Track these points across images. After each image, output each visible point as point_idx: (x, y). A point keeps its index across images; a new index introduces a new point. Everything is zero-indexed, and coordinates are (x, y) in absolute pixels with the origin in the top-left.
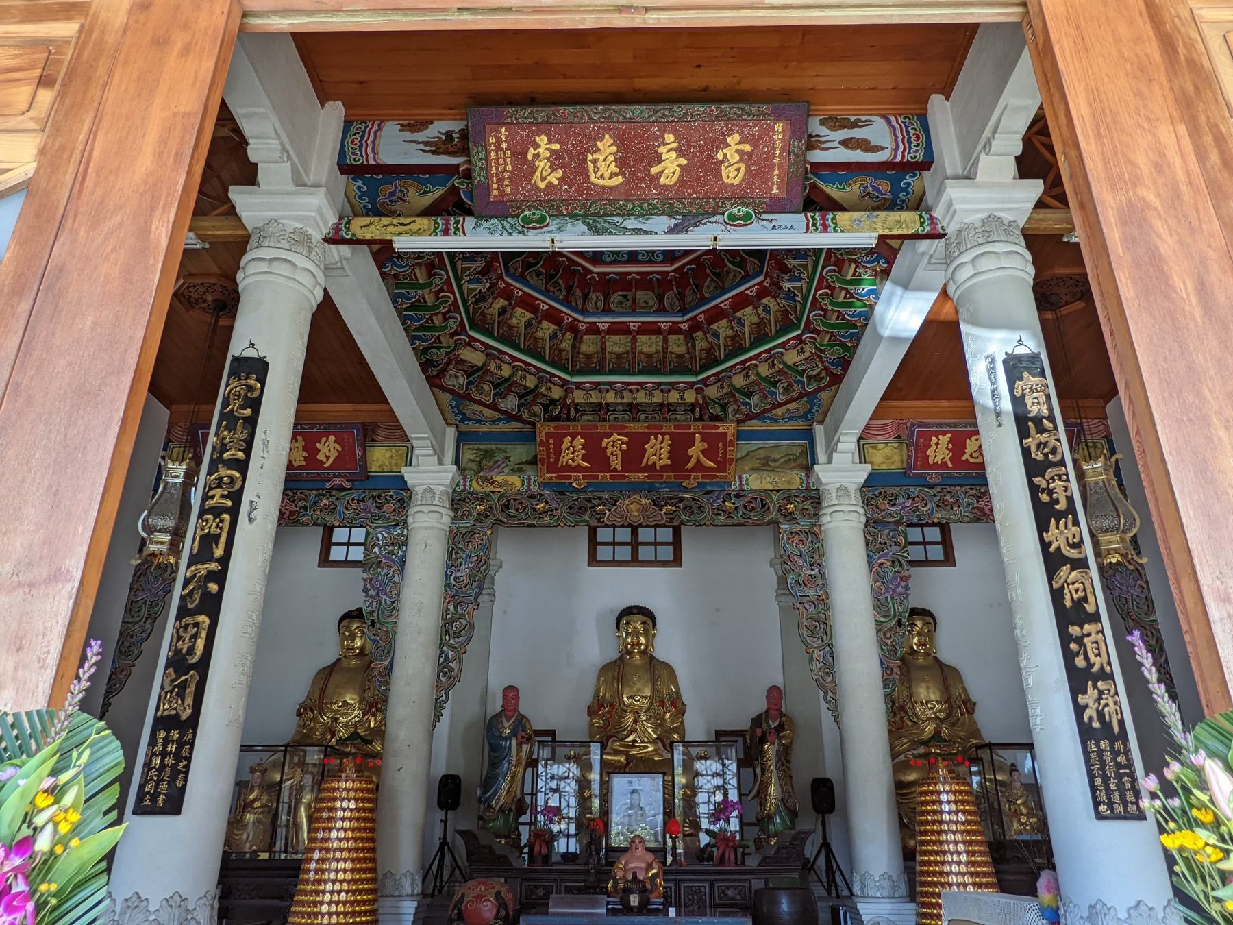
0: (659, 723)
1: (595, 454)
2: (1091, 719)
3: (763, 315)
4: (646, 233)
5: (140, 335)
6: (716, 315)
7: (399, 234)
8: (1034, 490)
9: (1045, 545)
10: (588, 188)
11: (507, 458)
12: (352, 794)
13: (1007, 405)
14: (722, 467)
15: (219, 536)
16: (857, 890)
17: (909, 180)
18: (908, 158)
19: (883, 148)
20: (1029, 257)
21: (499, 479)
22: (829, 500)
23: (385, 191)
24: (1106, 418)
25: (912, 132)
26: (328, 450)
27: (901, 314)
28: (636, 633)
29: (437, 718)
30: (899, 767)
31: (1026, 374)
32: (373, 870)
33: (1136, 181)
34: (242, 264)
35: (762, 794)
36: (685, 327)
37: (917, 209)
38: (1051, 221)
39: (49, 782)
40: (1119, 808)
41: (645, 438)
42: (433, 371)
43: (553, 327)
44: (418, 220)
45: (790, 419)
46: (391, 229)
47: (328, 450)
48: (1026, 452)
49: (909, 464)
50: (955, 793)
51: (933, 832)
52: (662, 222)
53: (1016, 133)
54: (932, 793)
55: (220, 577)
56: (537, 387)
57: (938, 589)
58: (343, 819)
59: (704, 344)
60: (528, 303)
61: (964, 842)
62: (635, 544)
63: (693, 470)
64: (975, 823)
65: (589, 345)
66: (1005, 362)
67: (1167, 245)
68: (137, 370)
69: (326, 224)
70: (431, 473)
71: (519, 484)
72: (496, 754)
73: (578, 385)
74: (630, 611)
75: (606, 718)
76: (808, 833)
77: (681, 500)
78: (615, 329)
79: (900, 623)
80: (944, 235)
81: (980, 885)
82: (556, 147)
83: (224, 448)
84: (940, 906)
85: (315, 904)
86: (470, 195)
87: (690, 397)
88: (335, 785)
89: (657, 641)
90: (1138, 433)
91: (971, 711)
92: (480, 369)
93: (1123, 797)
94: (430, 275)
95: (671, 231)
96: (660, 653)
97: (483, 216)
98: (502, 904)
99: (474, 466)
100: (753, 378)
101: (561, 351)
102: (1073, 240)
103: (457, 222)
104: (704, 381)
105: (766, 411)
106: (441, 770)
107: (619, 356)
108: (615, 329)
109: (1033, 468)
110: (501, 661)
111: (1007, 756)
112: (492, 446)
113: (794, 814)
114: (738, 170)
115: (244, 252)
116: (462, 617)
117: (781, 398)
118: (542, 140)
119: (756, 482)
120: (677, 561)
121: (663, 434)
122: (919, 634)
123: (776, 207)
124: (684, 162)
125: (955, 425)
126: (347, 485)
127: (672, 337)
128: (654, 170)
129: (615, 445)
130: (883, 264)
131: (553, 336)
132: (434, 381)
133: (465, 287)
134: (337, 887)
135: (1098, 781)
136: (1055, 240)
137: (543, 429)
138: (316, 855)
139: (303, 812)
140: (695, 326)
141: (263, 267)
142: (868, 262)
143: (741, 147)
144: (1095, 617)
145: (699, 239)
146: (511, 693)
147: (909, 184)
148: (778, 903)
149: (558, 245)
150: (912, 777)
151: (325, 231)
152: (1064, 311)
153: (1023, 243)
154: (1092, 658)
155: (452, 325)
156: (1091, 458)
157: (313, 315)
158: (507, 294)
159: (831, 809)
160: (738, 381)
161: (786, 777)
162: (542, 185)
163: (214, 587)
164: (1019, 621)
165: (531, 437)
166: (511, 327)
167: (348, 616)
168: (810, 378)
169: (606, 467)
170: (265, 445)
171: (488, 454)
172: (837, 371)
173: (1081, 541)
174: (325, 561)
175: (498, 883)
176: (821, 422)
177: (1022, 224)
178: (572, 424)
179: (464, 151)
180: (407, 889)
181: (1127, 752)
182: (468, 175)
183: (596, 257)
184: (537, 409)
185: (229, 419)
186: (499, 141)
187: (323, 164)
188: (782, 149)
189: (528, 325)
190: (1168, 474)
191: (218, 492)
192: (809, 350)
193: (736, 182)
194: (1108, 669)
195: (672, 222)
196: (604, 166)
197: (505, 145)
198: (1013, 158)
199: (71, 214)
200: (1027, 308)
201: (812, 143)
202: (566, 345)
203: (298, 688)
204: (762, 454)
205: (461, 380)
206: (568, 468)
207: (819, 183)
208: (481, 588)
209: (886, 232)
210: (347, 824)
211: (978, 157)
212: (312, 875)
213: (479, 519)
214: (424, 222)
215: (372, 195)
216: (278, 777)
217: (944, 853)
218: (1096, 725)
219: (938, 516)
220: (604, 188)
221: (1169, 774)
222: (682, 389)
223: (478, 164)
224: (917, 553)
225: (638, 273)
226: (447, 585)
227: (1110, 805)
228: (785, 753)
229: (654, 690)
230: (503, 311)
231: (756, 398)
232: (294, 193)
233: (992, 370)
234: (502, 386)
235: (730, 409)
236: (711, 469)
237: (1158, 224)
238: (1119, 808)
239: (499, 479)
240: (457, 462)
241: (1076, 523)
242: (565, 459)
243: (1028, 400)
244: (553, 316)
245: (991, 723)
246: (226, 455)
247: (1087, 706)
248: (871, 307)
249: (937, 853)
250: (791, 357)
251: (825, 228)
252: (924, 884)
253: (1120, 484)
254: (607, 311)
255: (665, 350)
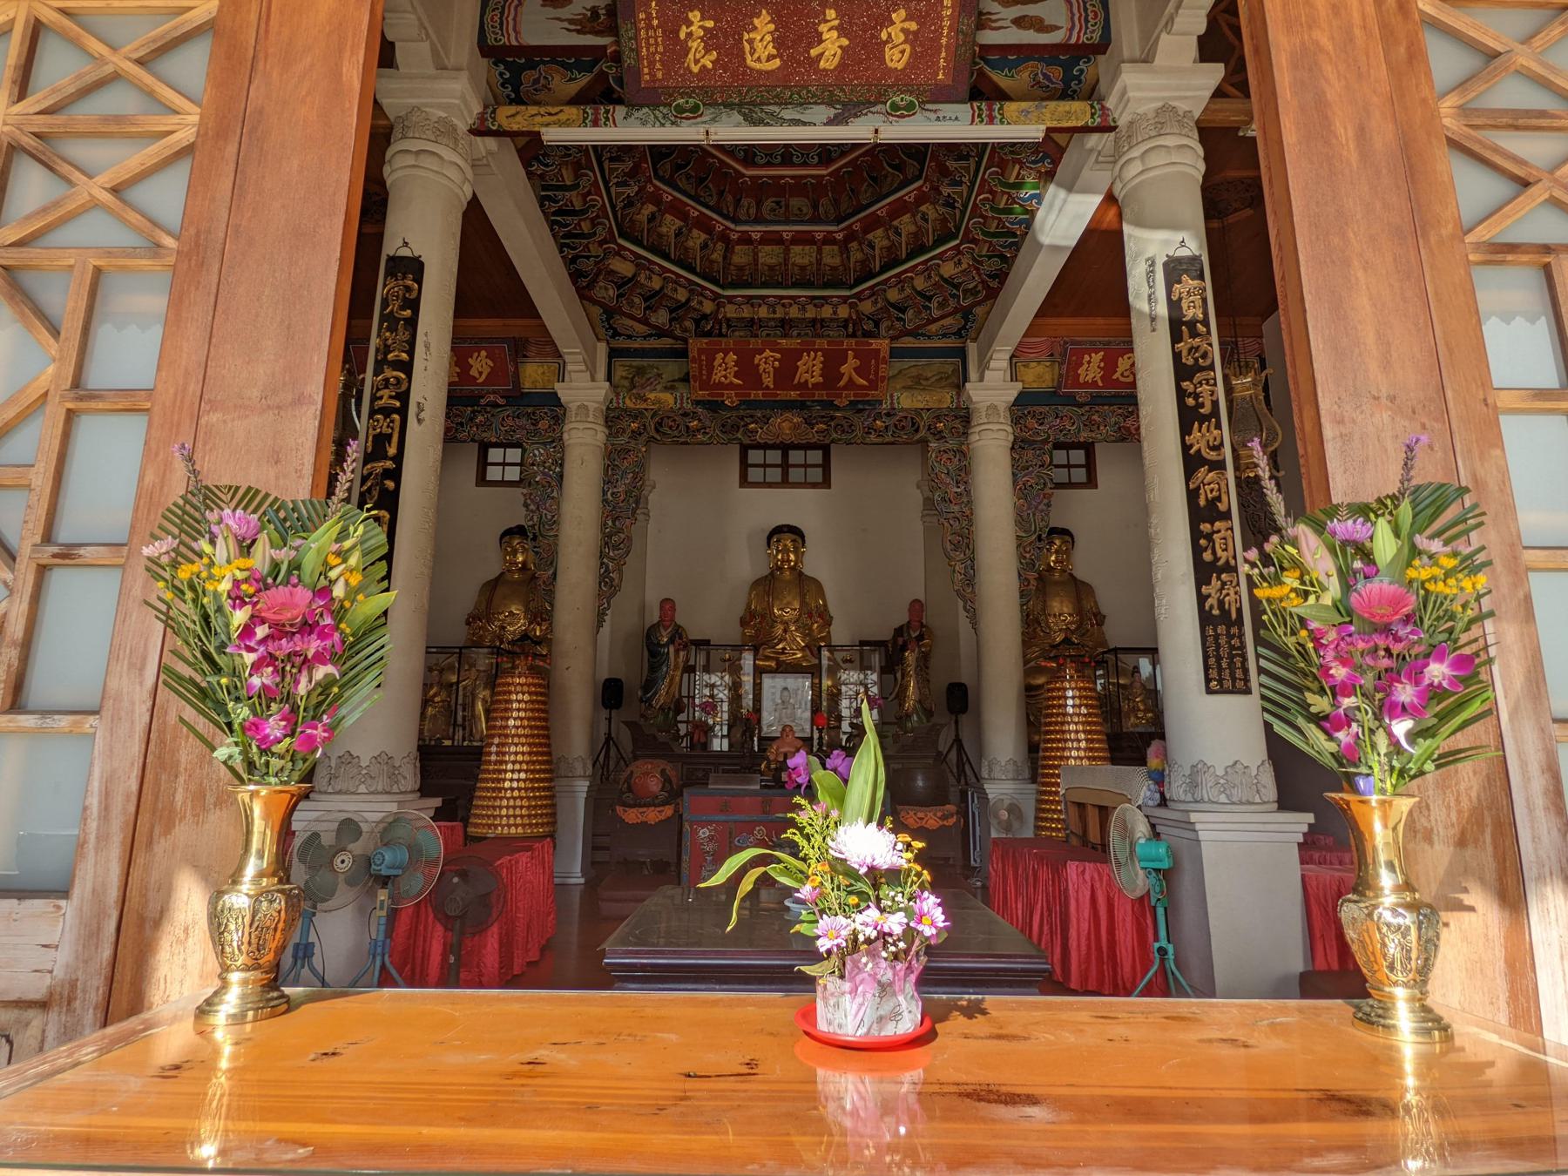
0: (806, 632)
1: (747, 370)
2: (1211, 607)
3: (921, 222)
4: (805, 124)
5: (346, 178)
6: (872, 223)
7: (547, 125)
8: (1181, 394)
9: (1186, 448)
10: (744, 73)
11: (659, 375)
12: (525, 689)
13: (1162, 310)
14: (873, 385)
15: (390, 436)
16: (985, 774)
17: (1082, 66)
18: (1083, 39)
19: (1058, 28)
20: (1201, 151)
21: (652, 396)
22: (979, 418)
23: (528, 77)
24: (1261, 337)
25: (1090, 8)
26: (480, 365)
27: (1062, 218)
28: (786, 551)
29: (600, 623)
30: (1030, 670)
31: (1185, 277)
32: (549, 754)
33: (1312, 23)
34: (388, 157)
35: (901, 696)
36: (840, 236)
37: (1089, 98)
38: (1229, 112)
39: (336, 547)
40: (1228, 684)
41: (798, 355)
42: (583, 282)
43: (704, 236)
44: (566, 108)
45: (944, 335)
46: (538, 119)
47: (480, 365)
48: (1177, 356)
49: (1060, 383)
50: (1079, 689)
51: (1056, 723)
52: (822, 112)
53: (1200, 8)
54: (1059, 689)
55: (396, 474)
56: (688, 300)
57: (1079, 511)
58: (519, 710)
59: (859, 256)
60: (677, 210)
61: (1084, 732)
62: (785, 466)
63: (845, 388)
64: (1096, 715)
65: (741, 256)
66: (1165, 265)
67: (1334, 89)
68: (347, 213)
69: (470, 112)
70: (584, 390)
71: (671, 401)
72: (655, 654)
73: (730, 299)
74: (779, 530)
75: (757, 632)
76: (942, 726)
77: (833, 418)
78: (768, 239)
79: (1039, 538)
80: (1115, 128)
81: (1094, 758)
82: (710, 24)
83: (387, 349)
84: (1058, 785)
85: (499, 781)
86: (620, 81)
87: (843, 312)
88: (510, 680)
89: (806, 559)
90: (1283, 278)
91: (1100, 623)
92: (630, 280)
93: (1233, 675)
94: (577, 176)
95: (830, 122)
96: (808, 570)
97: (634, 105)
98: (667, 780)
99: (626, 383)
100: (908, 291)
101: (712, 262)
102: (1250, 134)
103: (607, 112)
104: (856, 296)
105: (919, 327)
106: (604, 674)
107: (771, 268)
108: (768, 239)
109: (1183, 372)
110: (658, 575)
111: (1128, 659)
112: (645, 362)
113: (929, 713)
114: (903, 52)
115: (389, 143)
116: (621, 531)
117: (936, 313)
118: (695, 16)
119: (907, 401)
120: (826, 483)
121: (816, 351)
122: (1057, 552)
123: (941, 95)
124: (845, 42)
125: (1109, 343)
126: (501, 401)
127: (827, 248)
128: (813, 52)
129: (767, 361)
130: (1048, 165)
131: (704, 246)
132: (584, 294)
133: (613, 190)
134: (517, 767)
135: (1212, 661)
136: (1230, 132)
137: (695, 345)
138: (496, 741)
139: (480, 707)
140: (851, 236)
141: (410, 160)
142: (1034, 162)
143: (906, 25)
144: (1227, 516)
145: (860, 131)
146: (667, 605)
147: (1081, 71)
148: (915, 780)
149: (713, 137)
150: (1041, 680)
151: (470, 122)
152: (1231, 219)
153: (1196, 136)
154: (1219, 553)
155: (601, 233)
156: (1241, 373)
157: (465, 214)
158: (656, 199)
159: (964, 710)
160: (893, 295)
161: (924, 681)
162: (695, 69)
163: (390, 484)
164: (1154, 520)
165: (683, 353)
166: (660, 236)
167: (509, 532)
168: (966, 291)
169: (758, 383)
170: (427, 347)
171: (640, 371)
172: (995, 280)
173: (1222, 444)
174: (482, 480)
175: (662, 764)
176: (975, 340)
177: (1197, 115)
178: (724, 340)
179: (613, 30)
180: (580, 771)
181: (1241, 636)
182: (617, 58)
183: (749, 154)
184: (688, 324)
185: (390, 320)
186: (649, 17)
187: (463, 46)
188: (950, 28)
189: (678, 234)
190: (1305, 311)
191: (386, 393)
192: (966, 261)
193: (900, 66)
194: (1232, 562)
195: (832, 112)
196: (761, 47)
197: (655, 22)
198: (1195, 39)
199: (261, 55)
200: (1192, 207)
201: (982, 21)
202: (717, 256)
203: (466, 598)
204: (914, 372)
205: (611, 292)
206: (720, 385)
207: (987, 69)
208: (637, 502)
209: (1054, 124)
210: (522, 714)
211: (1158, 38)
212: (493, 758)
213: (634, 438)
214: (572, 112)
215: (515, 83)
216: (454, 679)
217: (1066, 741)
218: (1216, 612)
219: (1084, 436)
220: (760, 72)
221: (1268, 548)
222: (836, 305)
223: (627, 45)
224: (1061, 475)
225: (792, 177)
226: (605, 501)
227: (1220, 682)
228: (924, 660)
229: (803, 603)
230: (652, 218)
231: (910, 313)
232: (435, 78)
233: (1150, 273)
234: (653, 299)
235: (884, 325)
236: (862, 387)
237: (1328, 69)
238: (1228, 684)
239: (652, 396)
240: (609, 379)
241: (1218, 426)
242: (718, 376)
243: (1184, 305)
244: (704, 224)
245: (1117, 632)
246: (390, 356)
247: (1209, 596)
248: (1032, 214)
249: (1059, 741)
250: (948, 270)
251: (991, 120)
252: (1045, 767)
253: (1267, 398)
254: (758, 220)
255: (819, 262)
